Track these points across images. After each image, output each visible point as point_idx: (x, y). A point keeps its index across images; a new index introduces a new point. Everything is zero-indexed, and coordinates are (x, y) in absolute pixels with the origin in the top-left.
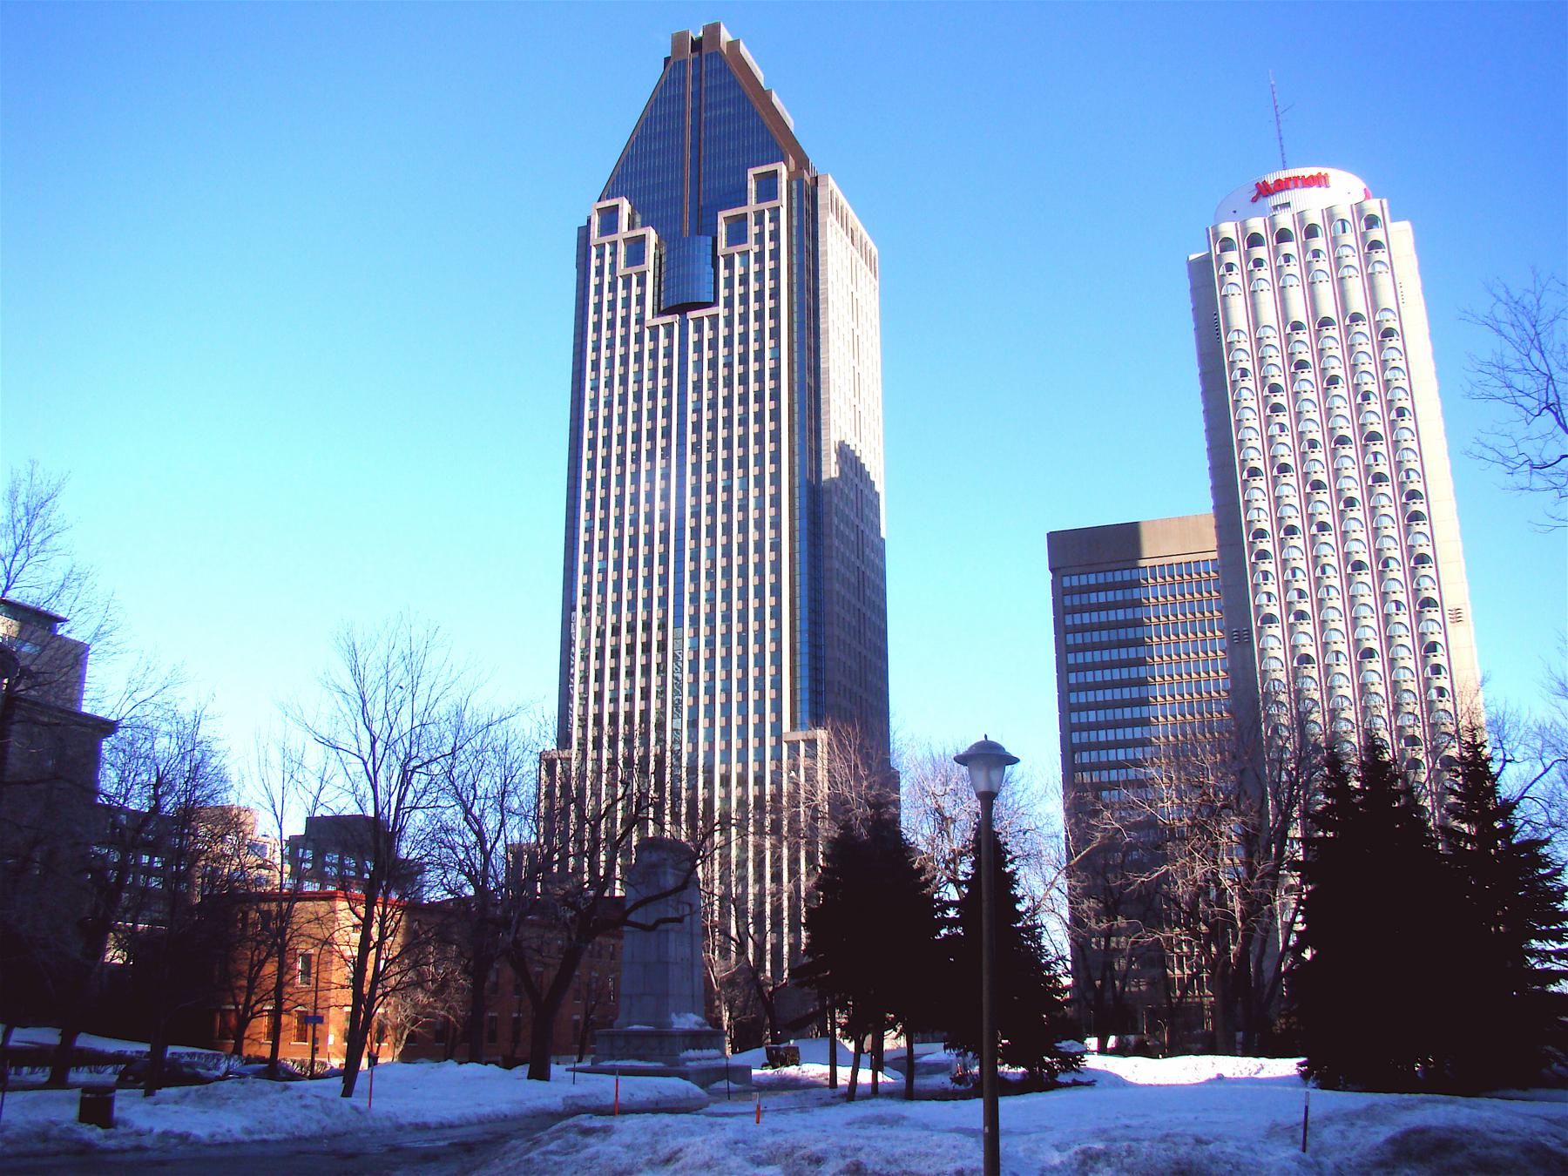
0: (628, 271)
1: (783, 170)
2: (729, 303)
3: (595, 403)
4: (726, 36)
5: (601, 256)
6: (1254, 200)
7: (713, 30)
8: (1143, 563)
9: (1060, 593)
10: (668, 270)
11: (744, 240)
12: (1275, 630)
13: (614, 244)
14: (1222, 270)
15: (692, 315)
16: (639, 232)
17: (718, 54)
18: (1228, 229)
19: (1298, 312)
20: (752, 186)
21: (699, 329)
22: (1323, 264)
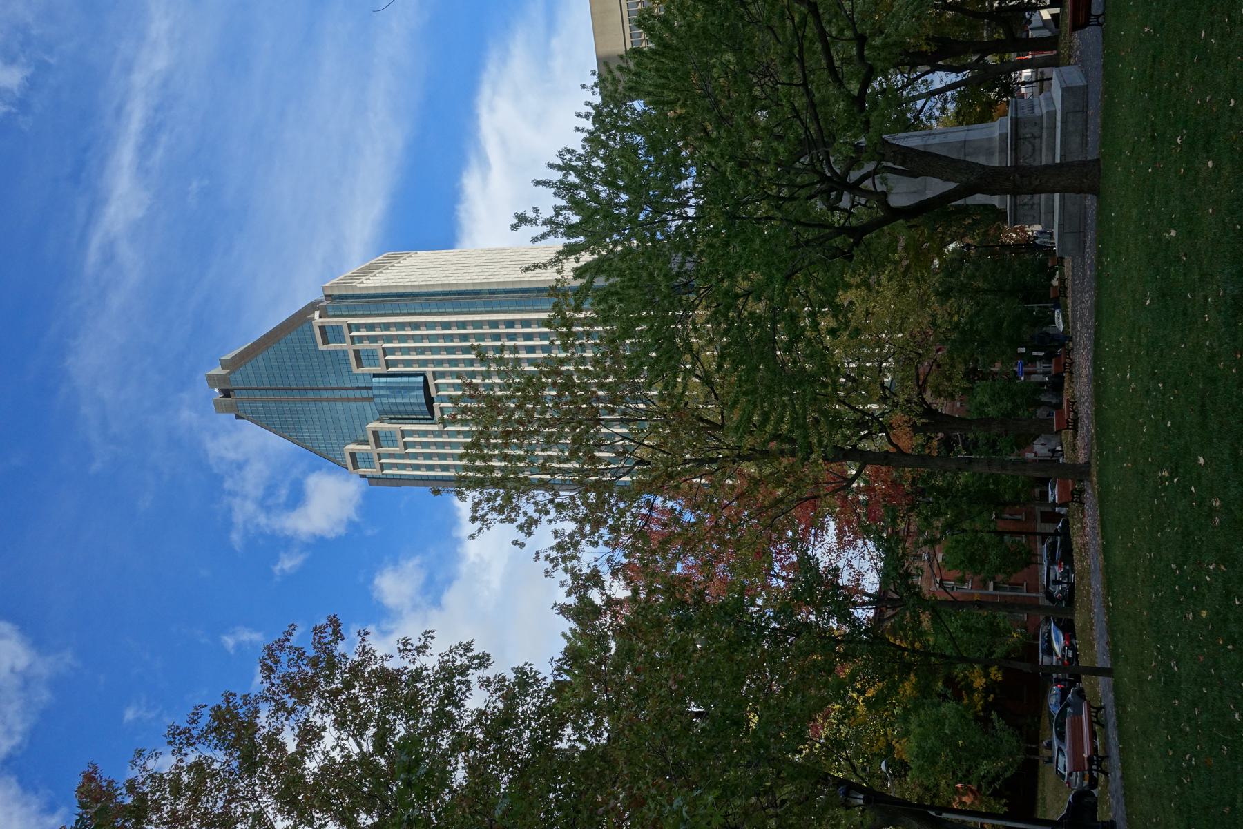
2: (425, 363)
20: (332, 346)
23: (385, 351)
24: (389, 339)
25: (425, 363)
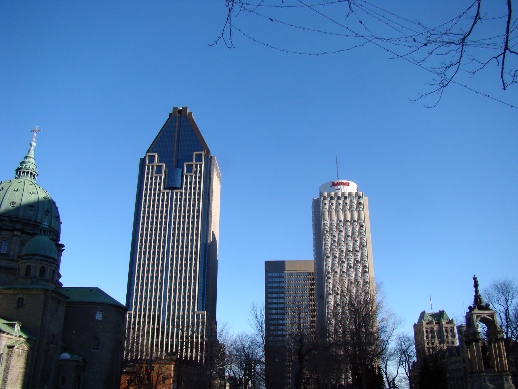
0: (156, 175)
1: (204, 154)
2: (186, 189)
3: (144, 211)
4: (188, 111)
5: (148, 169)
6: (331, 186)
7: (185, 109)
8: (285, 272)
9: (267, 278)
10: (168, 176)
11: (191, 172)
12: (331, 297)
13: (153, 166)
14: (323, 205)
15: (175, 191)
16: (161, 164)
17: (186, 116)
18: (326, 194)
19: (341, 218)
20: (195, 157)
21: (177, 195)
22: (348, 207)
23: (191, 176)
24: (195, 178)
25: (186, 189)
